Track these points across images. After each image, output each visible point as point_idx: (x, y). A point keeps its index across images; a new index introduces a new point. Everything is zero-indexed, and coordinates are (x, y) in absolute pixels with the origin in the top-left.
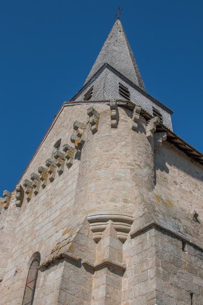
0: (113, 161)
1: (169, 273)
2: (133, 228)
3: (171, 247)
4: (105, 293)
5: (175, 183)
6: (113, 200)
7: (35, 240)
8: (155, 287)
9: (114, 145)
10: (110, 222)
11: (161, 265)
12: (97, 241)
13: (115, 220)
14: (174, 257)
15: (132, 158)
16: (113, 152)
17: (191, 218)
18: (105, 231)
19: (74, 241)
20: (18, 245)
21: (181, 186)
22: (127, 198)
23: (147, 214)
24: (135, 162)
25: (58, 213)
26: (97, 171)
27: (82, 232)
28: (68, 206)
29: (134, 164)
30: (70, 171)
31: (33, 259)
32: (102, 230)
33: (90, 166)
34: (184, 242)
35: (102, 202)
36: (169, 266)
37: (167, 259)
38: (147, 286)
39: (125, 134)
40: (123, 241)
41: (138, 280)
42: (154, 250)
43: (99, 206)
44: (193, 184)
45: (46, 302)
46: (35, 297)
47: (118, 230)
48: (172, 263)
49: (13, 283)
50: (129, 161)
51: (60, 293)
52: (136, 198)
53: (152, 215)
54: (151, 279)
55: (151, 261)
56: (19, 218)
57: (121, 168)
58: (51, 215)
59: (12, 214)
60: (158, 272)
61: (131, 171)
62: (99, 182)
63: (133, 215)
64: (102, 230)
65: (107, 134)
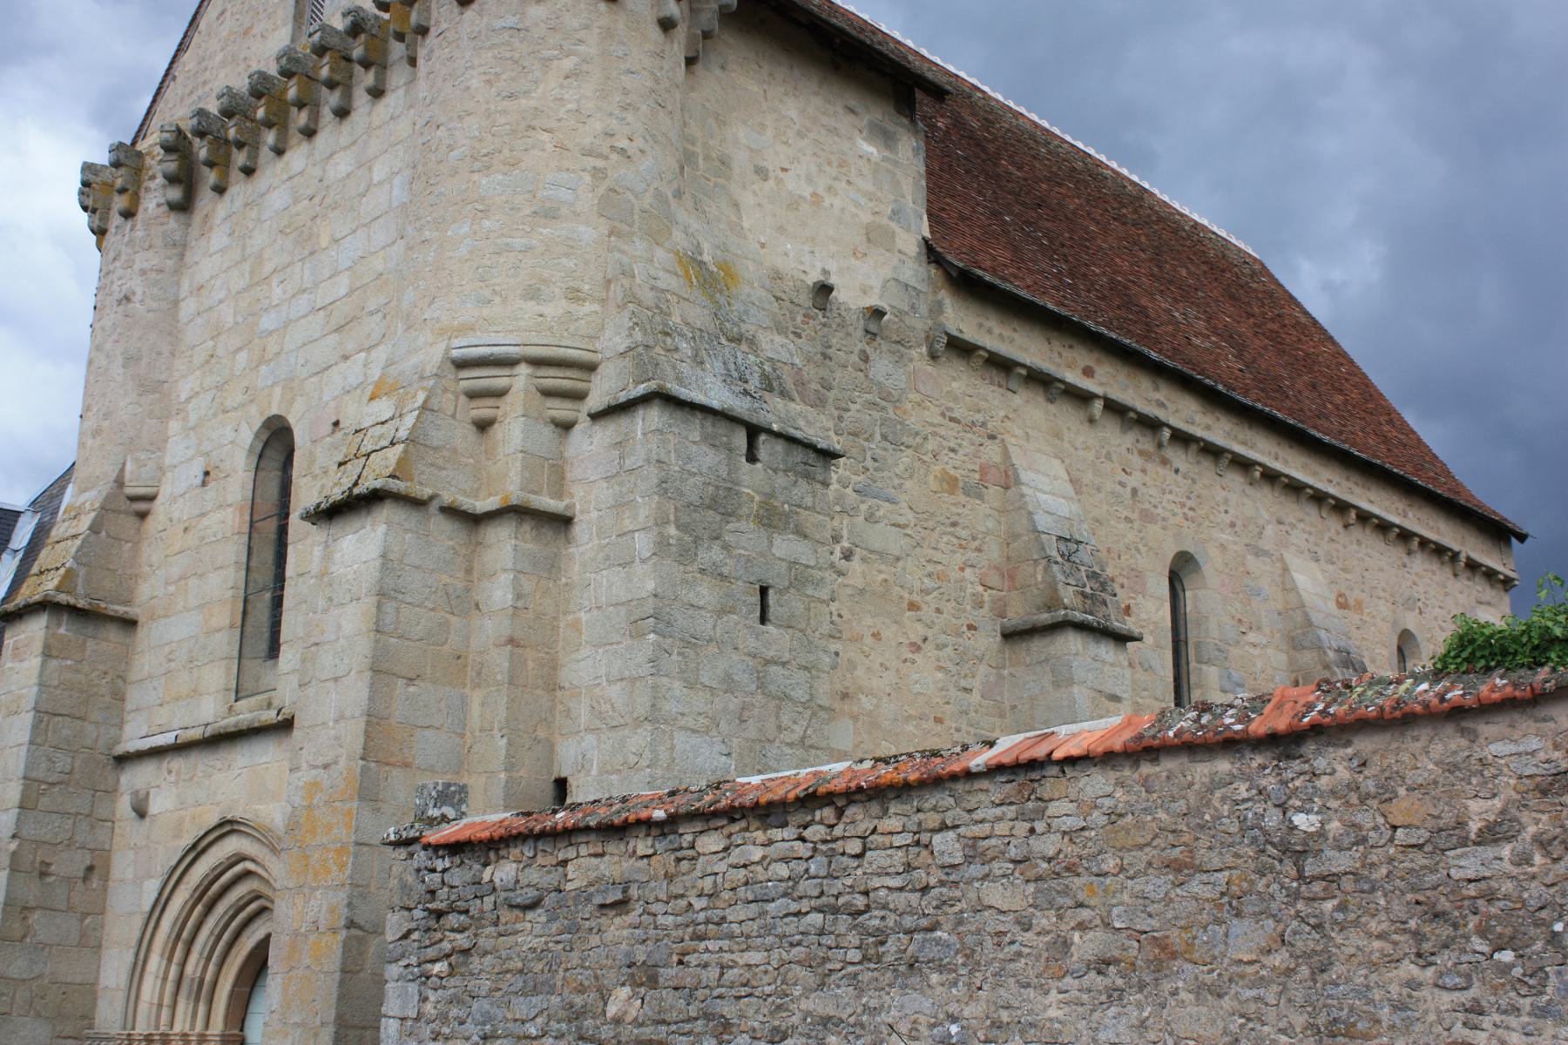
0: (530, 141)
1: (697, 541)
2: (602, 391)
3: (704, 456)
4: (510, 596)
5: (762, 173)
6: (532, 294)
7: (263, 369)
8: (650, 585)
9: (537, 74)
10: (523, 370)
11: (672, 518)
12: (483, 426)
13: (537, 362)
14: (717, 488)
15: (598, 126)
16: (532, 103)
17: (805, 299)
18: (509, 398)
19: (411, 440)
20: (198, 373)
21: (779, 181)
22: (576, 284)
23: (640, 349)
24: (609, 142)
25: (342, 285)
26: (476, 177)
27: (434, 403)
28: (380, 268)
29: (606, 151)
30: (376, 121)
31: (264, 437)
32: (500, 394)
33: (451, 148)
34: (754, 431)
35: (497, 300)
36: (696, 516)
37: (694, 498)
38: (631, 581)
39: (576, 25)
40: (566, 427)
41: (607, 558)
42: (653, 474)
43: (486, 312)
44: (830, 164)
45: (339, 627)
46: (290, 571)
47: (548, 393)
48: (709, 507)
49: (203, 515)
50: (587, 141)
51: (379, 607)
52: (609, 281)
53: (658, 350)
54: (643, 561)
55: (645, 508)
56: (189, 258)
57: (560, 169)
58: (316, 285)
59: (158, 242)
60: (662, 546)
61: (593, 176)
62: (487, 223)
63: (598, 346)
64: (500, 394)
65: (511, 21)
